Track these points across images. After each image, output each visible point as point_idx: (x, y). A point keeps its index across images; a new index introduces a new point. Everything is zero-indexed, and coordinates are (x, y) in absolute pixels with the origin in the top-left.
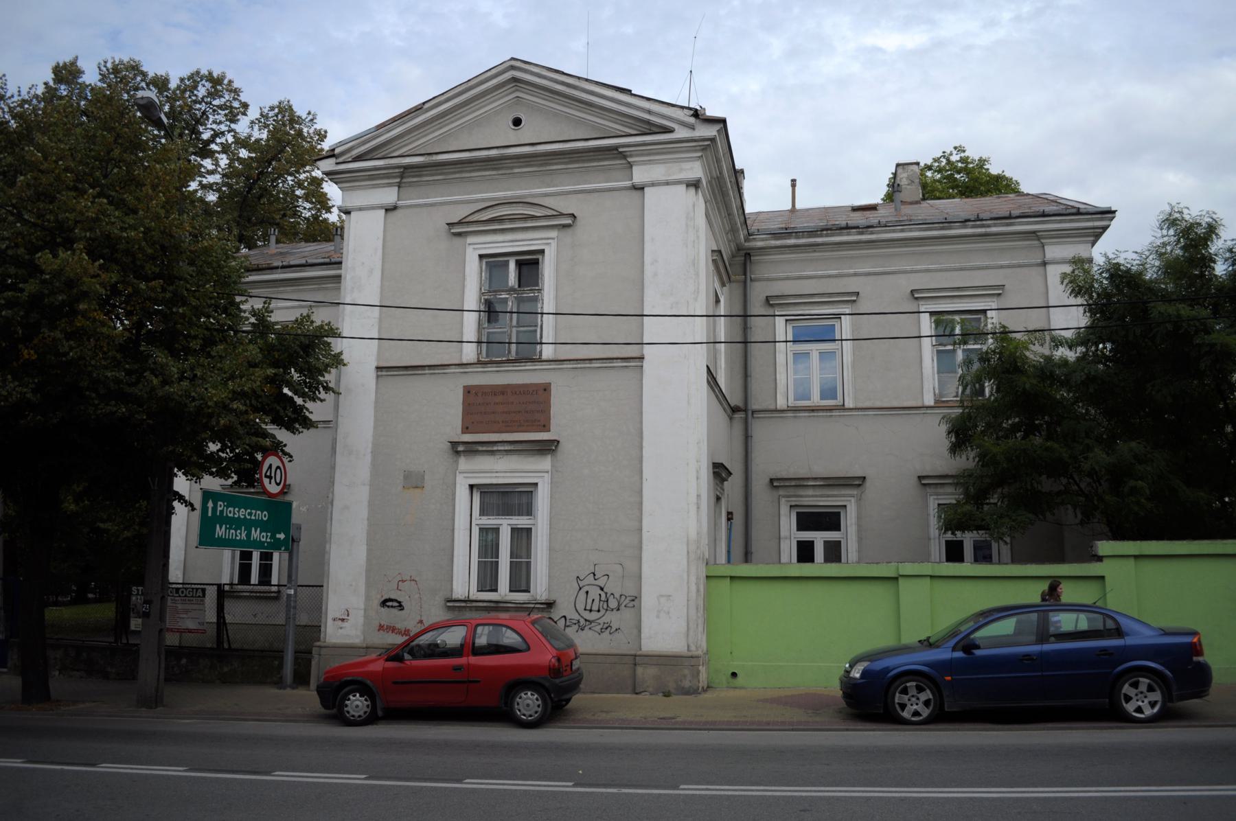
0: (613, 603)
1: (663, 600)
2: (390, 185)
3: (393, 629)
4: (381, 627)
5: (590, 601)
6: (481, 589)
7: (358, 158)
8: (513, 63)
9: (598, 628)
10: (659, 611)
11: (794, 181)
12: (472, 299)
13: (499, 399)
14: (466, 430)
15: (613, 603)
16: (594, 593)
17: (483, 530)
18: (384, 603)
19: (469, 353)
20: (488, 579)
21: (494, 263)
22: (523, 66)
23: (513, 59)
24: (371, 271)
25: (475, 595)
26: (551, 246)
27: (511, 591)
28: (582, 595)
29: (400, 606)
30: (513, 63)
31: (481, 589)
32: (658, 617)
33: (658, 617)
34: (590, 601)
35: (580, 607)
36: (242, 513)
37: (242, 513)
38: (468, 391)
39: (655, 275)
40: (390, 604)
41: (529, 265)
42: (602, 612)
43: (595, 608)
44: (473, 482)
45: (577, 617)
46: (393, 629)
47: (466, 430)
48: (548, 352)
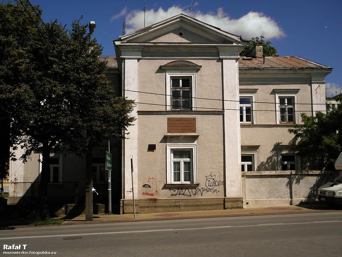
0: (217, 184)
1: (232, 182)
2: (139, 51)
3: (147, 194)
4: (143, 194)
5: (210, 183)
6: (175, 181)
7: (128, 42)
8: (182, 15)
9: (213, 191)
10: (231, 185)
11: (131, 159)
12: (169, 92)
13: (179, 122)
14: (169, 132)
15: (217, 184)
16: (211, 181)
17: (175, 163)
18: (144, 186)
19: (169, 108)
20: (177, 177)
21: (175, 81)
22: (185, 17)
23: (181, 14)
24: (134, 79)
25: (173, 182)
26: (195, 77)
27: (184, 181)
28: (208, 182)
29: (150, 187)
30: (182, 15)
31: (175, 181)
32: (231, 187)
33: (231, 187)
34: (210, 183)
35: (207, 185)
36: (16, 253)
37: (16, 253)
38: (169, 119)
39: (227, 86)
40: (146, 186)
41: (187, 82)
42: (214, 186)
43: (212, 185)
44: (172, 148)
45: (206, 188)
46: (147, 194)
47: (169, 132)
48: (193, 109)
